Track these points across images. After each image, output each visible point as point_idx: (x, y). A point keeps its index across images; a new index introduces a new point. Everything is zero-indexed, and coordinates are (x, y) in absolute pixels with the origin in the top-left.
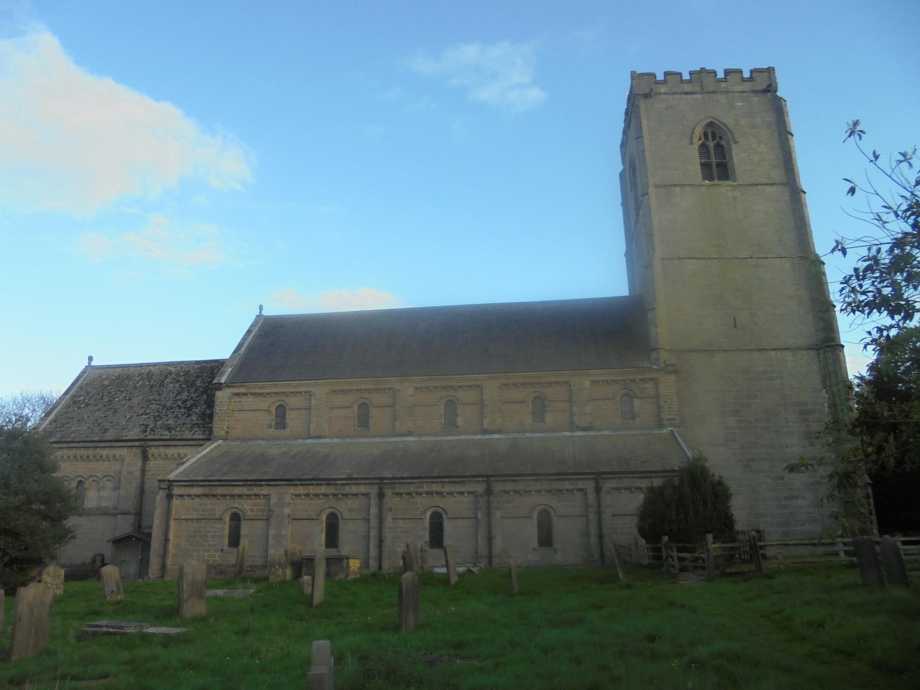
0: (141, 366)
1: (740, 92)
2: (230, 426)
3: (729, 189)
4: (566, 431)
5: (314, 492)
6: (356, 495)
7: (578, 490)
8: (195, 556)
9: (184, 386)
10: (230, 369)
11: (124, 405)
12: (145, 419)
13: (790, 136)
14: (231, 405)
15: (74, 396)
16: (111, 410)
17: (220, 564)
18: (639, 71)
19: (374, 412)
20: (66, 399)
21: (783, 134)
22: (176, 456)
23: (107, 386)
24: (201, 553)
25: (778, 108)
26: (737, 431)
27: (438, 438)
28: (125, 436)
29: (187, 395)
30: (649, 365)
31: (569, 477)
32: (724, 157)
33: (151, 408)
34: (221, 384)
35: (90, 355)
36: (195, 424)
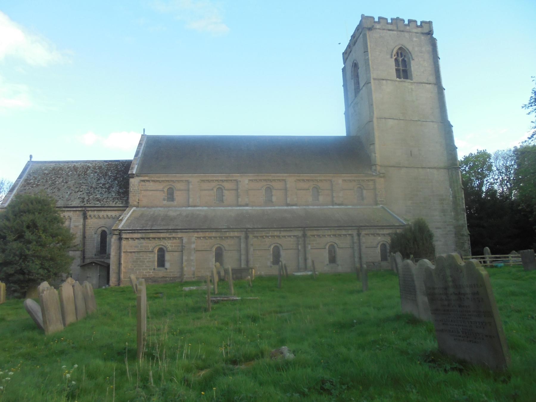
0: (68, 163)
1: (416, 33)
2: (140, 199)
3: (409, 84)
4: (330, 205)
5: (209, 235)
7: (349, 235)
8: (138, 273)
9: (101, 175)
10: (136, 166)
11: (64, 186)
12: (80, 194)
13: (439, 59)
14: (140, 187)
15: (26, 180)
16: (56, 189)
17: (154, 277)
18: (366, 14)
19: (226, 193)
22: (105, 216)
23: (47, 174)
24: (141, 271)
25: (433, 43)
26: (411, 208)
28: (71, 204)
29: (105, 180)
30: (372, 173)
31: (345, 228)
32: (406, 67)
33: (83, 188)
34: (134, 174)
35: (30, 154)
36: (115, 198)
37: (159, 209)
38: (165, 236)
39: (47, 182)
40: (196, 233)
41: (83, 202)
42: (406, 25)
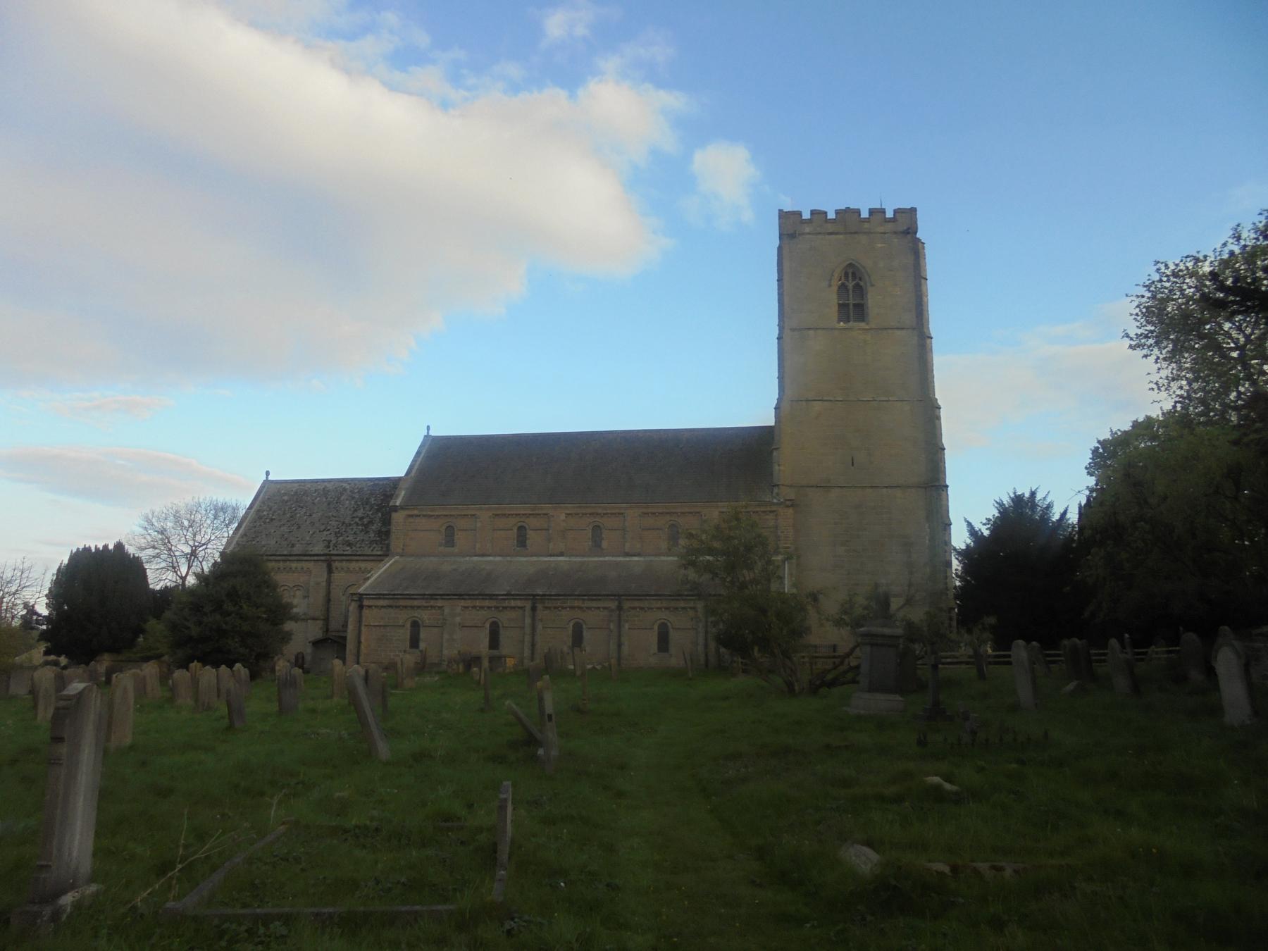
0: (317, 482)
1: (882, 233)
6: (514, 608)
10: (403, 493)
11: (306, 521)
19: (530, 534)
20: (251, 513)
21: (918, 277)
23: (287, 502)
25: (916, 250)
27: (586, 559)
36: (373, 541)
37: (432, 558)
38: (419, 605)
39: (284, 514)
40: (463, 601)
41: (329, 547)
42: (865, 220)
